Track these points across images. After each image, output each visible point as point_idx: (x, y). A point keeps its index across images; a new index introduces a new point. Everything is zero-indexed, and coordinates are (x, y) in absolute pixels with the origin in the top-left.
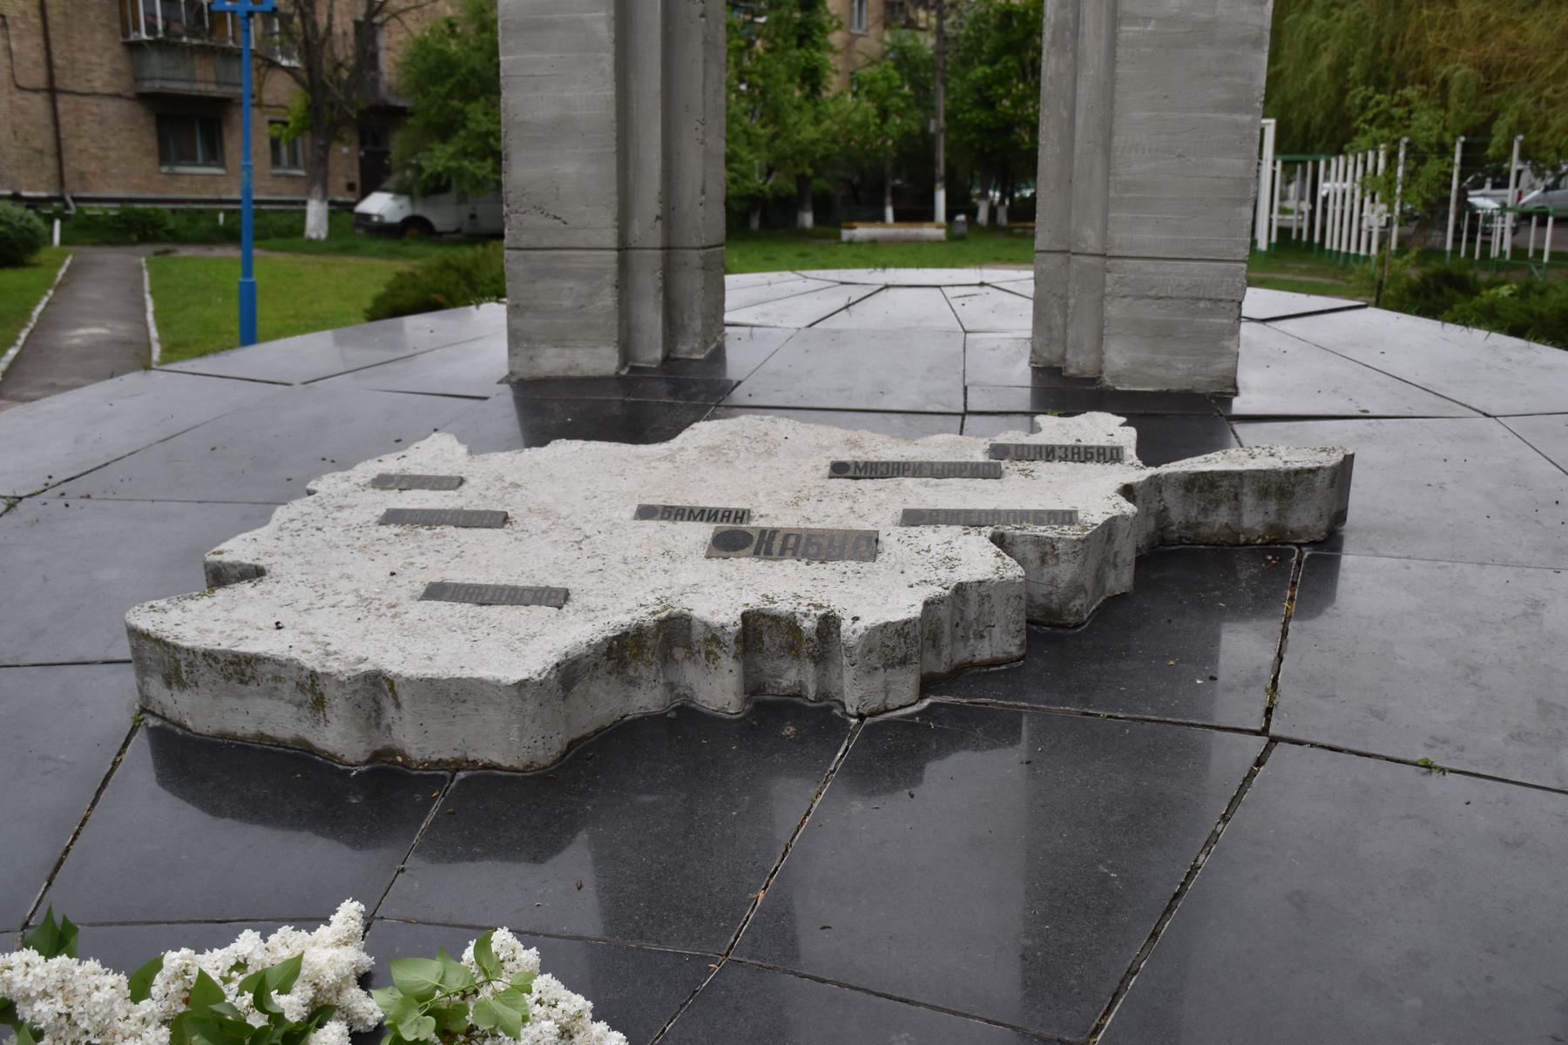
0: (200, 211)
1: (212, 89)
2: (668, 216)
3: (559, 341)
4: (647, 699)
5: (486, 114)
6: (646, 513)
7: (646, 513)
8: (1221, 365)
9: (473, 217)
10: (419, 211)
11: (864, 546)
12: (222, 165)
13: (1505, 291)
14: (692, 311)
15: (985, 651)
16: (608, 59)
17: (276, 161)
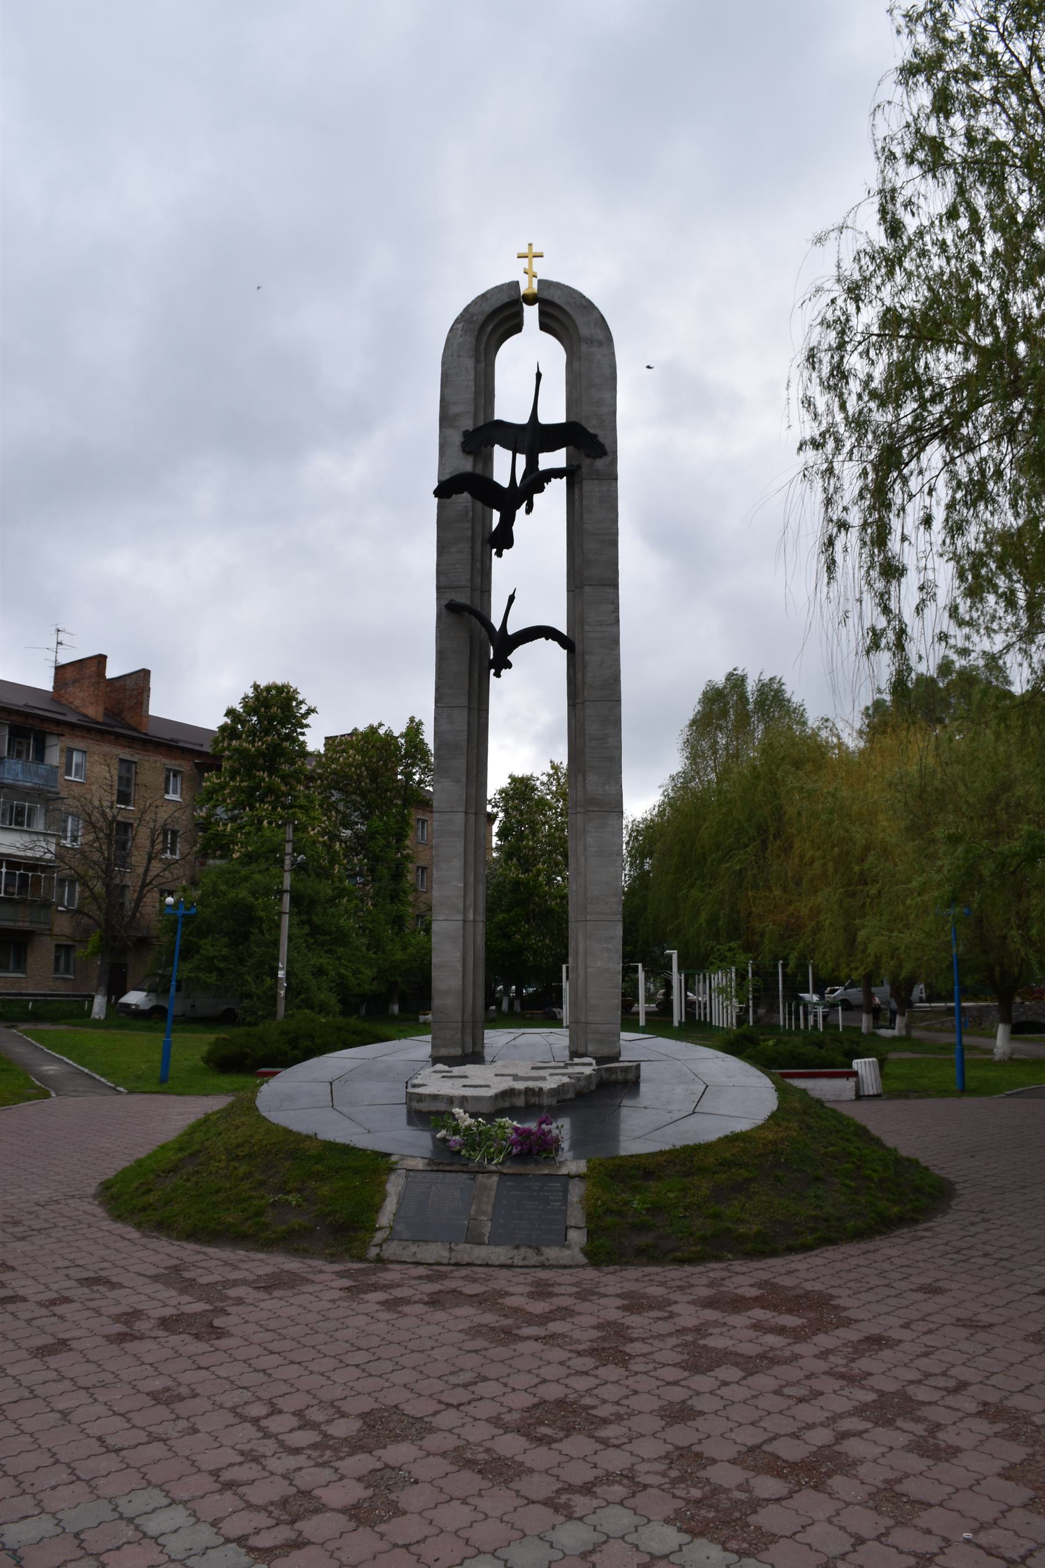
0: (11, 1001)
1: (27, 926)
2: (473, 1014)
3: (445, 1047)
4: (507, 1104)
5: (212, 946)
6: (496, 1075)
7: (496, 1075)
8: (617, 1050)
9: (193, 1006)
10: (161, 1003)
11: (544, 1079)
12: (24, 972)
13: (771, 1043)
14: (478, 1041)
15: (568, 1097)
16: (461, 975)
17: (57, 970)
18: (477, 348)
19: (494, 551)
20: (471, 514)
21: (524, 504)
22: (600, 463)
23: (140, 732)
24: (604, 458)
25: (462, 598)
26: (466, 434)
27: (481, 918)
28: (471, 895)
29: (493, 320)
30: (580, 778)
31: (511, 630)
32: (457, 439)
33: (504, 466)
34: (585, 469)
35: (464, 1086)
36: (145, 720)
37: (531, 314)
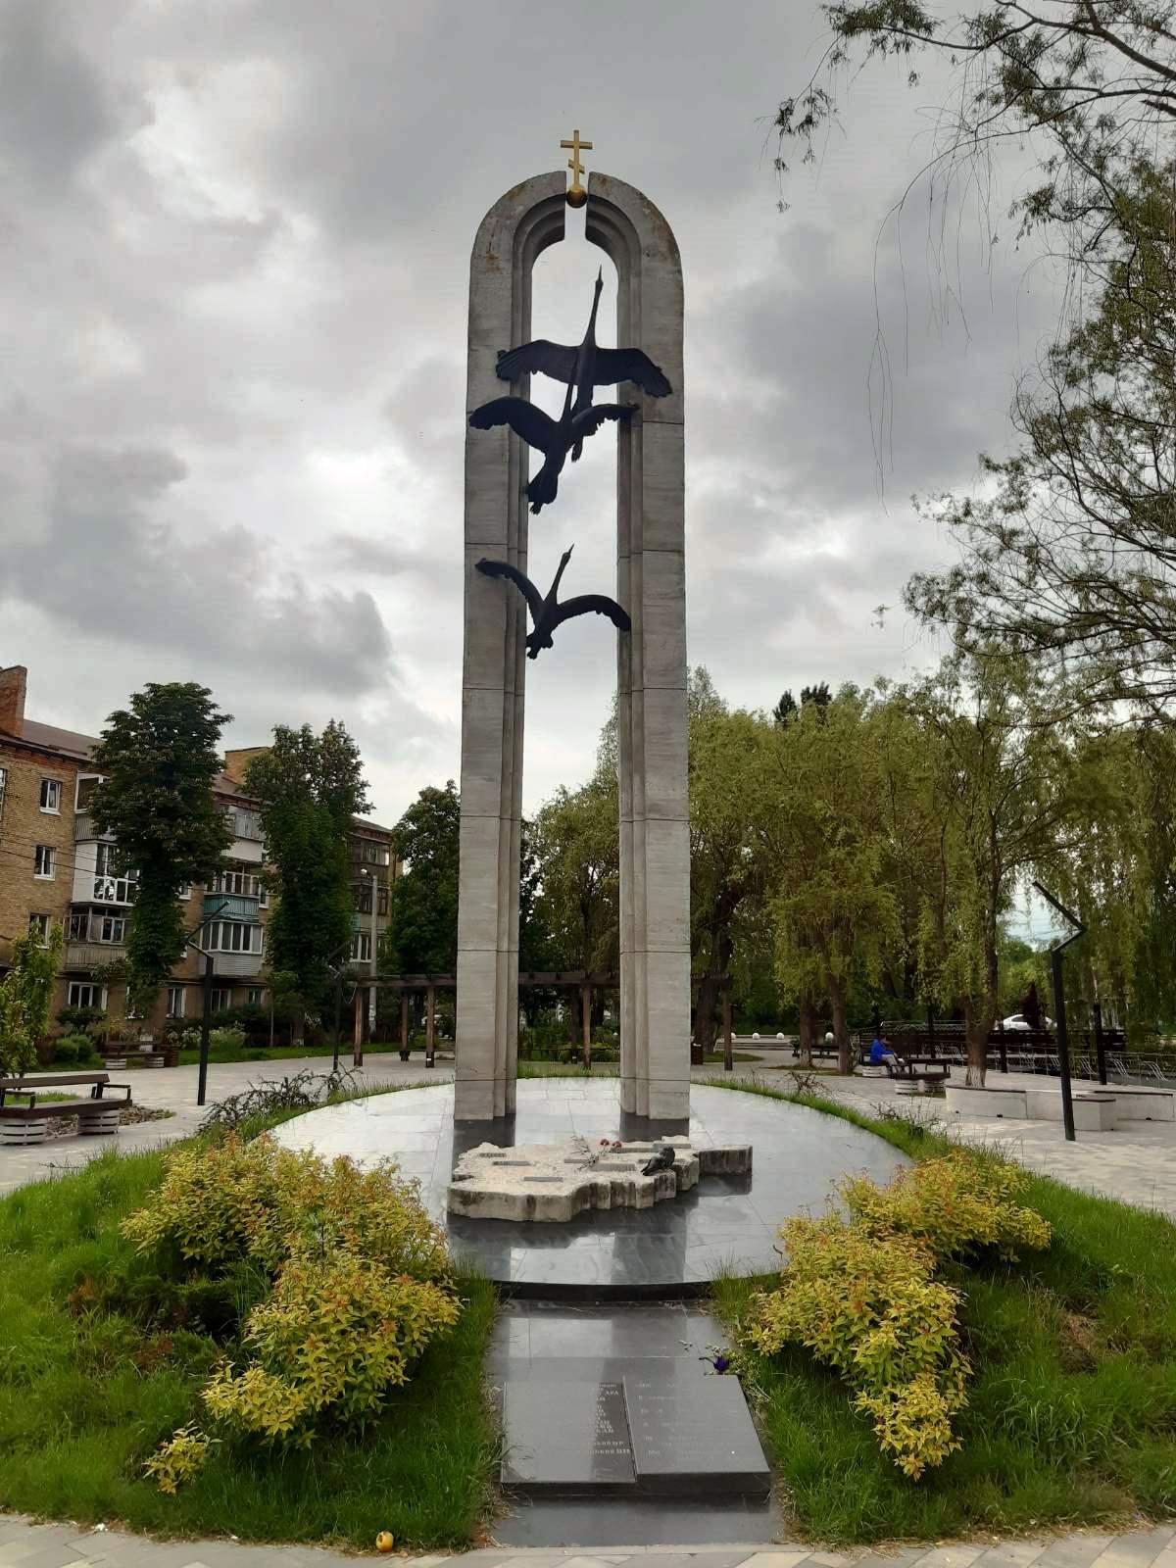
18: (514, 253)
19: (531, 504)
20: (507, 454)
21: (571, 450)
22: (662, 403)
23: (11, 736)
24: (669, 396)
25: (497, 555)
26: (501, 355)
27: (516, 947)
28: (506, 919)
29: (529, 222)
30: (636, 779)
31: (562, 598)
32: (490, 361)
33: (548, 395)
34: (644, 410)
35: (527, 1179)
36: (19, 723)
37: (575, 219)
